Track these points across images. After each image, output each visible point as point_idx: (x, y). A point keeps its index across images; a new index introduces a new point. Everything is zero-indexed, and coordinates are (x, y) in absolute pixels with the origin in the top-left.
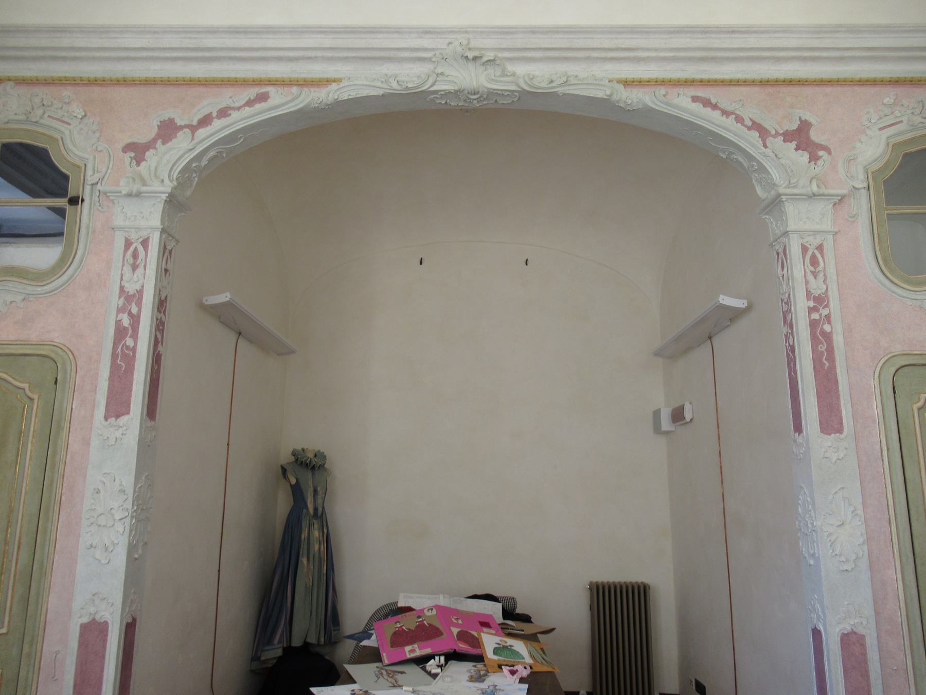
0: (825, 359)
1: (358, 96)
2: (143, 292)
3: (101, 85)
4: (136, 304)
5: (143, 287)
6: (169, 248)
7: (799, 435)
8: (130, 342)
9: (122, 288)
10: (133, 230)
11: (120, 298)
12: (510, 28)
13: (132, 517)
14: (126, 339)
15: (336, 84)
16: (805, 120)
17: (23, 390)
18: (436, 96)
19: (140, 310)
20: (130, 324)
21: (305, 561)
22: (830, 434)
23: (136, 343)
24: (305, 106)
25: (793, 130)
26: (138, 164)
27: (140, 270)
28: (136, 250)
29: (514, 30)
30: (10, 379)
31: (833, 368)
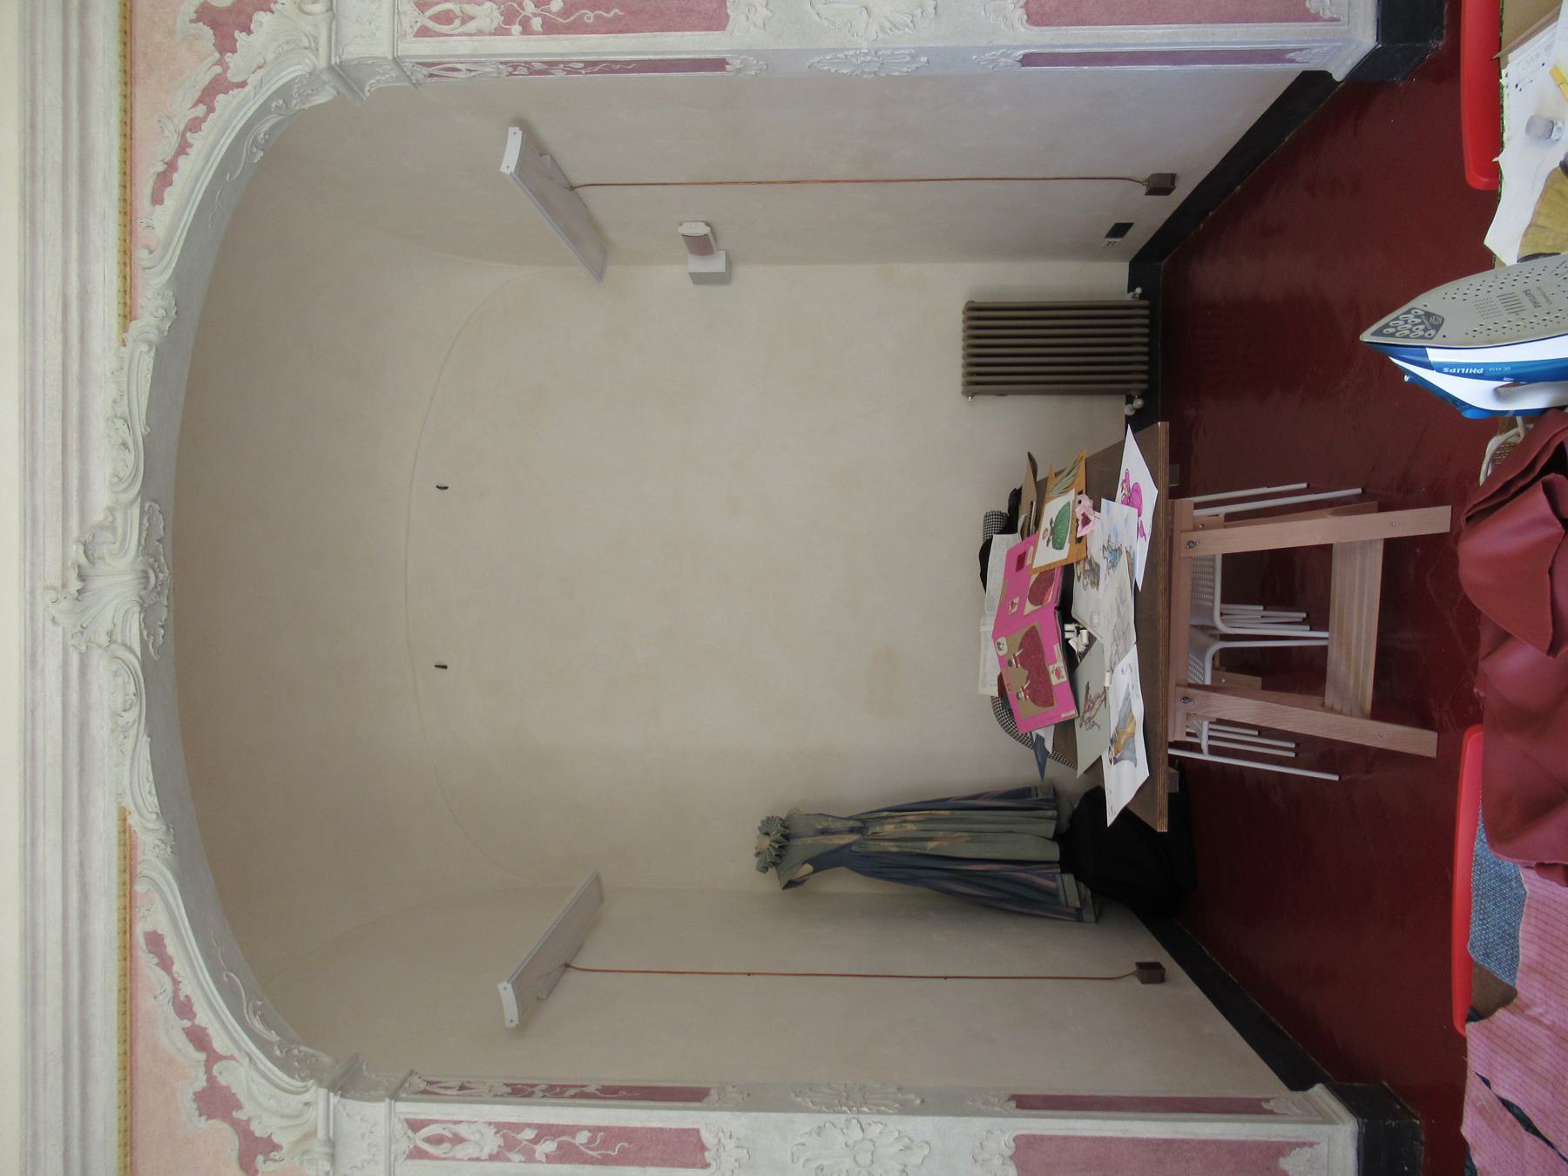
0: (608, 13)
5: (490, 1124)
6: (423, 1086)
11: (509, 1160)
12: (25, 517)
13: (859, 1112)
16: (195, 12)
21: (931, 845)
22: (728, 16)
25: (215, 34)
29: (28, 509)
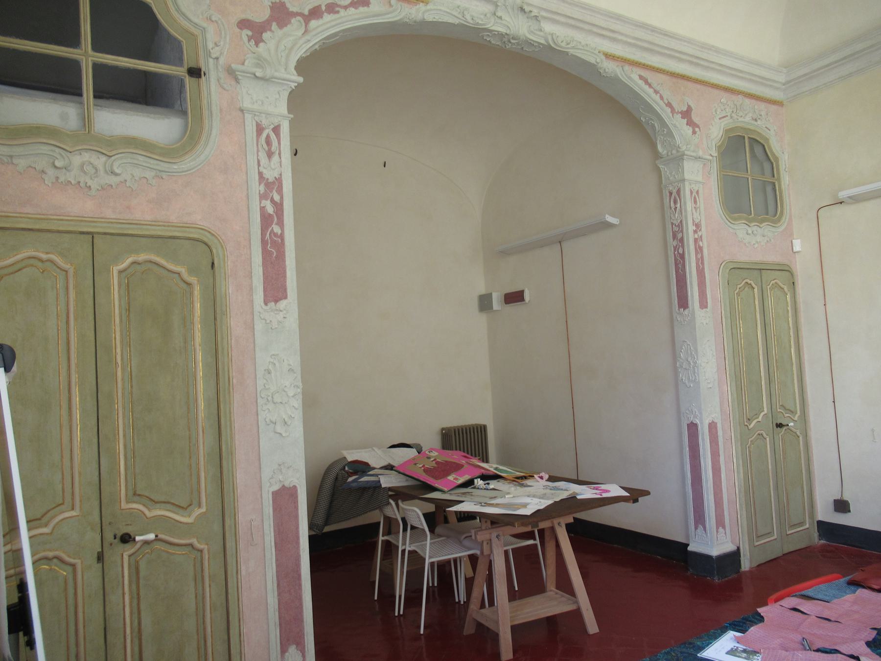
1: (440, 20)
2: (282, 181)
4: (276, 191)
5: (281, 175)
7: (684, 310)
8: (277, 229)
9: (261, 174)
10: (264, 115)
14: (273, 226)
15: (423, 4)
17: (64, 273)
18: (489, 34)
19: (282, 198)
20: (274, 212)
23: (282, 230)
24: (400, 20)
26: (257, 44)
27: (275, 158)
28: (268, 137)
30: (163, 262)
31: (703, 268)
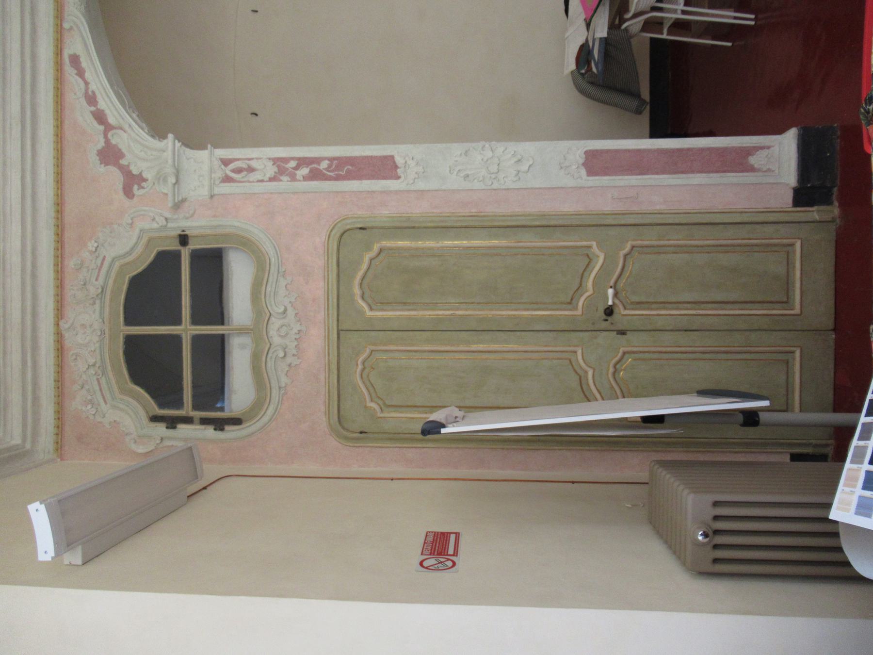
3: (63, 230)
11: (281, 180)
